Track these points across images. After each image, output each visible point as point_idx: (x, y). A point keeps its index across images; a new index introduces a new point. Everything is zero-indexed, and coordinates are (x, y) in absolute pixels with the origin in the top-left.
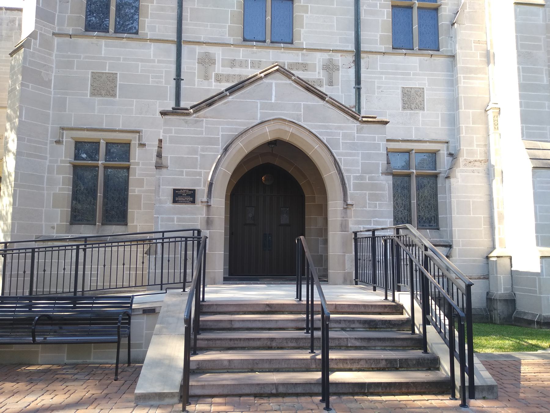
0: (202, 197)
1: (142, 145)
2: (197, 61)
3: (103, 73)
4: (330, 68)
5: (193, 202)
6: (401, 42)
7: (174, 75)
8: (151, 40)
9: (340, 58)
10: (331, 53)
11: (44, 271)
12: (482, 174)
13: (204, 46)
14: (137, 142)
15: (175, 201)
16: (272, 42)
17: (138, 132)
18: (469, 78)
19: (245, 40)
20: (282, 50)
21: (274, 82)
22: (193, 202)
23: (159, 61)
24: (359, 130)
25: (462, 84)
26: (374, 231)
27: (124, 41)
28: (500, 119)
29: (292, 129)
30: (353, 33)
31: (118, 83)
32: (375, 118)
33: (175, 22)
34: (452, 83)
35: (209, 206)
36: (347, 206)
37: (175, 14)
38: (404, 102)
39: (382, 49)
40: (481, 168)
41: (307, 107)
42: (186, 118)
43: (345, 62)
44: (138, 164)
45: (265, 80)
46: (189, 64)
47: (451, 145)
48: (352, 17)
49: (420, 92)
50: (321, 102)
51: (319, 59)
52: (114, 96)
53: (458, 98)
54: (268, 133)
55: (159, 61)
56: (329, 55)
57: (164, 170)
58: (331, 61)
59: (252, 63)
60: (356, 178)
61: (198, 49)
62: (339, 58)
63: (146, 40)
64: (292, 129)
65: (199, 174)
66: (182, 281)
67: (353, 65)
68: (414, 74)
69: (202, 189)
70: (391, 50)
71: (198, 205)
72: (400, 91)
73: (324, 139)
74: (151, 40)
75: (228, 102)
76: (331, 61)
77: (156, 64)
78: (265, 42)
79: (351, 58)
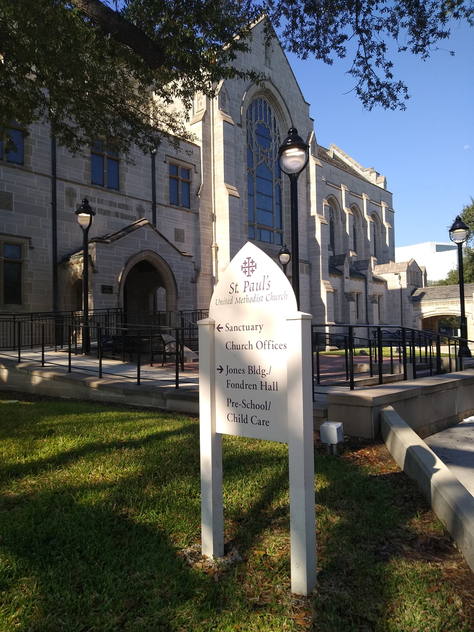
0: (116, 290)
1: (32, 248)
2: (65, 193)
3: (3, 192)
4: (140, 210)
5: (112, 293)
6: (175, 202)
7: (50, 200)
8: (35, 173)
9: (145, 205)
10: (140, 201)
11: (28, 332)
12: (209, 282)
13: (69, 183)
14: (28, 245)
15: (103, 292)
16: (108, 187)
17: (30, 238)
18: (204, 228)
19: (92, 183)
20: (115, 194)
21: (146, 229)
22: (112, 293)
23: (41, 189)
24: (181, 260)
25: (202, 231)
26: (108, 309)
27: (17, 170)
28: (219, 253)
29: (154, 256)
30: (151, 191)
31: (13, 201)
32: (185, 253)
33: (50, 162)
34: (197, 229)
35: (119, 296)
36: (177, 298)
37: (50, 156)
38: (175, 238)
39: (165, 202)
40: (209, 278)
41: (160, 245)
42: (107, 245)
43: (147, 207)
44: (29, 261)
45: (143, 228)
46: (61, 195)
47: (196, 264)
48: (150, 180)
49: (182, 232)
50: (166, 243)
51: (134, 203)
52: (11, 210)
53: (200, 238)
54: (143, 257)
55: (41, 189)
56: (140, 202)
57: (97, 274)
58: (140, 206)
59: (98, 199)
60: (181, 284)
61: (66, 185)
62: (144, 204)
63: (31, 172)
64: (154, 256)
65: (114, 277)
66: (41, 343)
67: (151, 210)
68: (180, 221)
69: (115, 286)
70: (169, 205)
71: (114, 295)
72: (174, 230)
73: (168, 262)
74: (35, 173)
75: (126, 238)
76: (140, 206)
77: (39, 190)
78: (103, 186)
79: (150, 206)
